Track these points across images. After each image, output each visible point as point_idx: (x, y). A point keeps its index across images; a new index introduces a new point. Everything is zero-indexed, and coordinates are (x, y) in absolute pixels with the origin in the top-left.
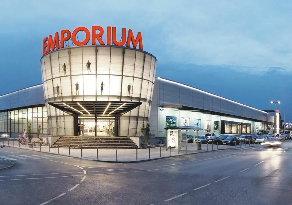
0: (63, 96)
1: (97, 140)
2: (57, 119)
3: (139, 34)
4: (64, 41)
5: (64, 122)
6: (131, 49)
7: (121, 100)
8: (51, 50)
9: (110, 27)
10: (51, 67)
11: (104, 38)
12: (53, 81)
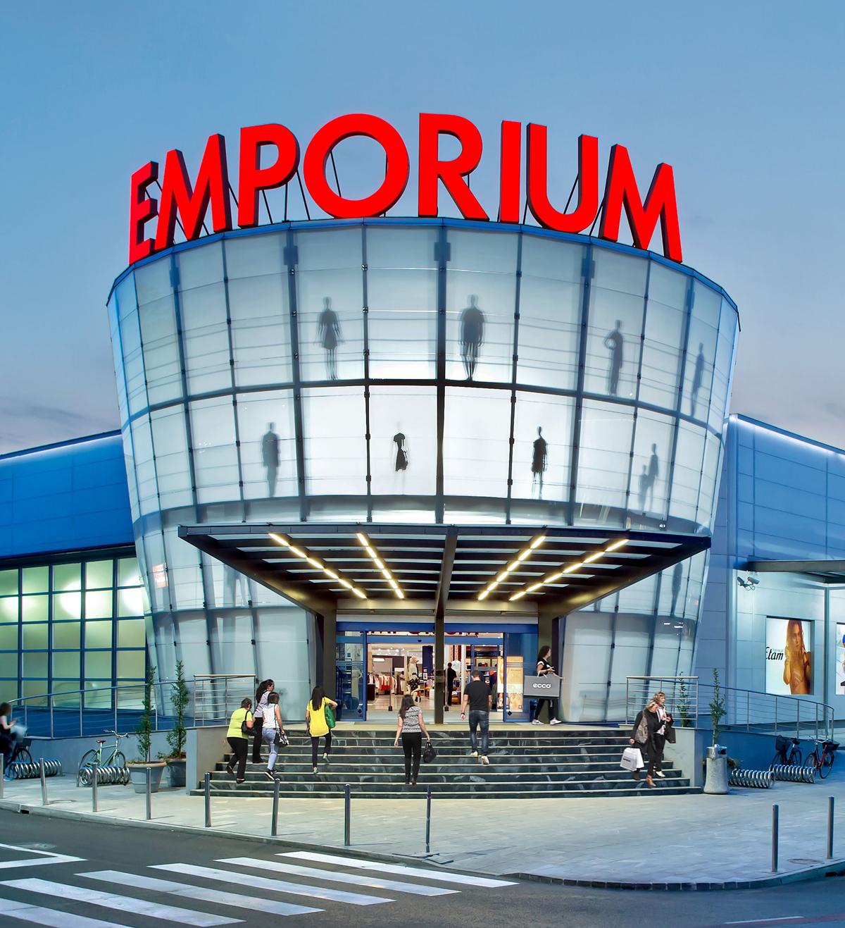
0: (248, 496)
1: (460, 743)
2: (211, 627)
3: (663, 174)
4: (258, 189)
5: (254, 642)
6: (623, 250)
7: (570, 524)
8: (180, 237)
9: (518, 125)
10: (180, 332)
11: (485, 185)
12: (187, 411)
